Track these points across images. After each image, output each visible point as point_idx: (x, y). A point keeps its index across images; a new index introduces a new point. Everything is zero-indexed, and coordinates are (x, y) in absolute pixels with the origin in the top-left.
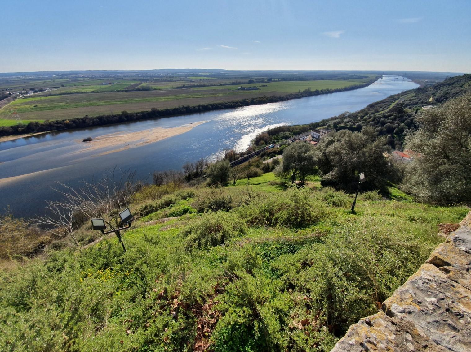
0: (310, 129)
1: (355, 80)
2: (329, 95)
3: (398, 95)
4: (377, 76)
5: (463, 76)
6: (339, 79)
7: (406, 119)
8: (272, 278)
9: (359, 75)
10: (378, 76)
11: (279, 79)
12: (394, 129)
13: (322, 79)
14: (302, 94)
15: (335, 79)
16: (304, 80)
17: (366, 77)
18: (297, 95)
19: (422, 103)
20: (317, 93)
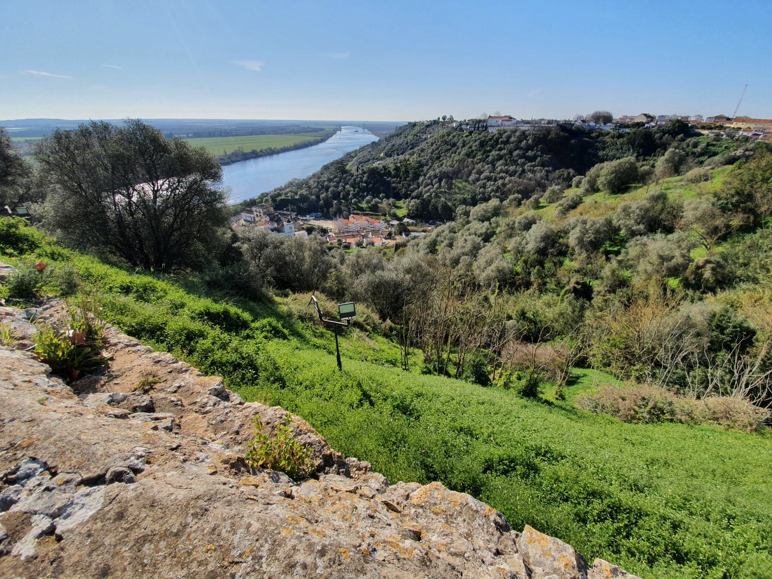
0: (243, 210)
1: (309, 134)
2: (275, 156)
3: (355, 151)
4: (335, 127)
5: (407, 126)
6: (287, 133)
7: (349, 179)
8: (499, 418)
9: (313, 127)
10: (336, 128)
11: (187, 134)
12: (339, 193)
13: (263, 133)
14: (229, 158)
15: (282, 134)
16: (234, 136)
17: (322, 130)
18: (223, 159)
19: (373, 159)
20: (255, 155)
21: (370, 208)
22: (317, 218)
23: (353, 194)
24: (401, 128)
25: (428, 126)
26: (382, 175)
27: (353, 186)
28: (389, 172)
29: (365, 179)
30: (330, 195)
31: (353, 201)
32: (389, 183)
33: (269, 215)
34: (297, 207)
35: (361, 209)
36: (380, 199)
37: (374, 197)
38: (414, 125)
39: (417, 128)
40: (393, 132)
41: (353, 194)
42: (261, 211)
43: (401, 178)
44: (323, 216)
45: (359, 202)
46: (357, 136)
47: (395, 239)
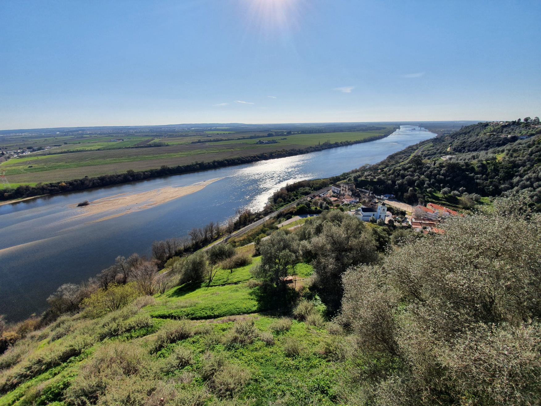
1: (374, 131)
2: (349, 147)
3: (417, 145)
4: (395, 126)
5: (477, 125)
6: (358, 130)
7: (425, 171)
9: (377, 126)
10: (395, 127)
11: (298, 132)
14: (321, 146)
15: (354, 131)
17: (384, 128)
18: (317, 148)
19: (440, 153)
21: (446, 198)
22: (390, 199)
23: (428, 184)
24: (467, 127)
25: (504, 126)
26: (464, 171)
27: (429, 177)
28: (473, 168)
29: (442, 172)
30: (406, 182)
31: (428, 190)
32: (472, 178)
33: (352, 191)
34: (374, 187)
35: (437, 198)
36: (459, 191)
37: (453, 189)
38: (486, 125)
39: (488, 129)
40: (458, 130)
41: (428, 184)
42: (347, 187)
43: (487, 175)
44: (396, 198)
45: (435, 192)
46: (414, 132)
47: (266, 189)
